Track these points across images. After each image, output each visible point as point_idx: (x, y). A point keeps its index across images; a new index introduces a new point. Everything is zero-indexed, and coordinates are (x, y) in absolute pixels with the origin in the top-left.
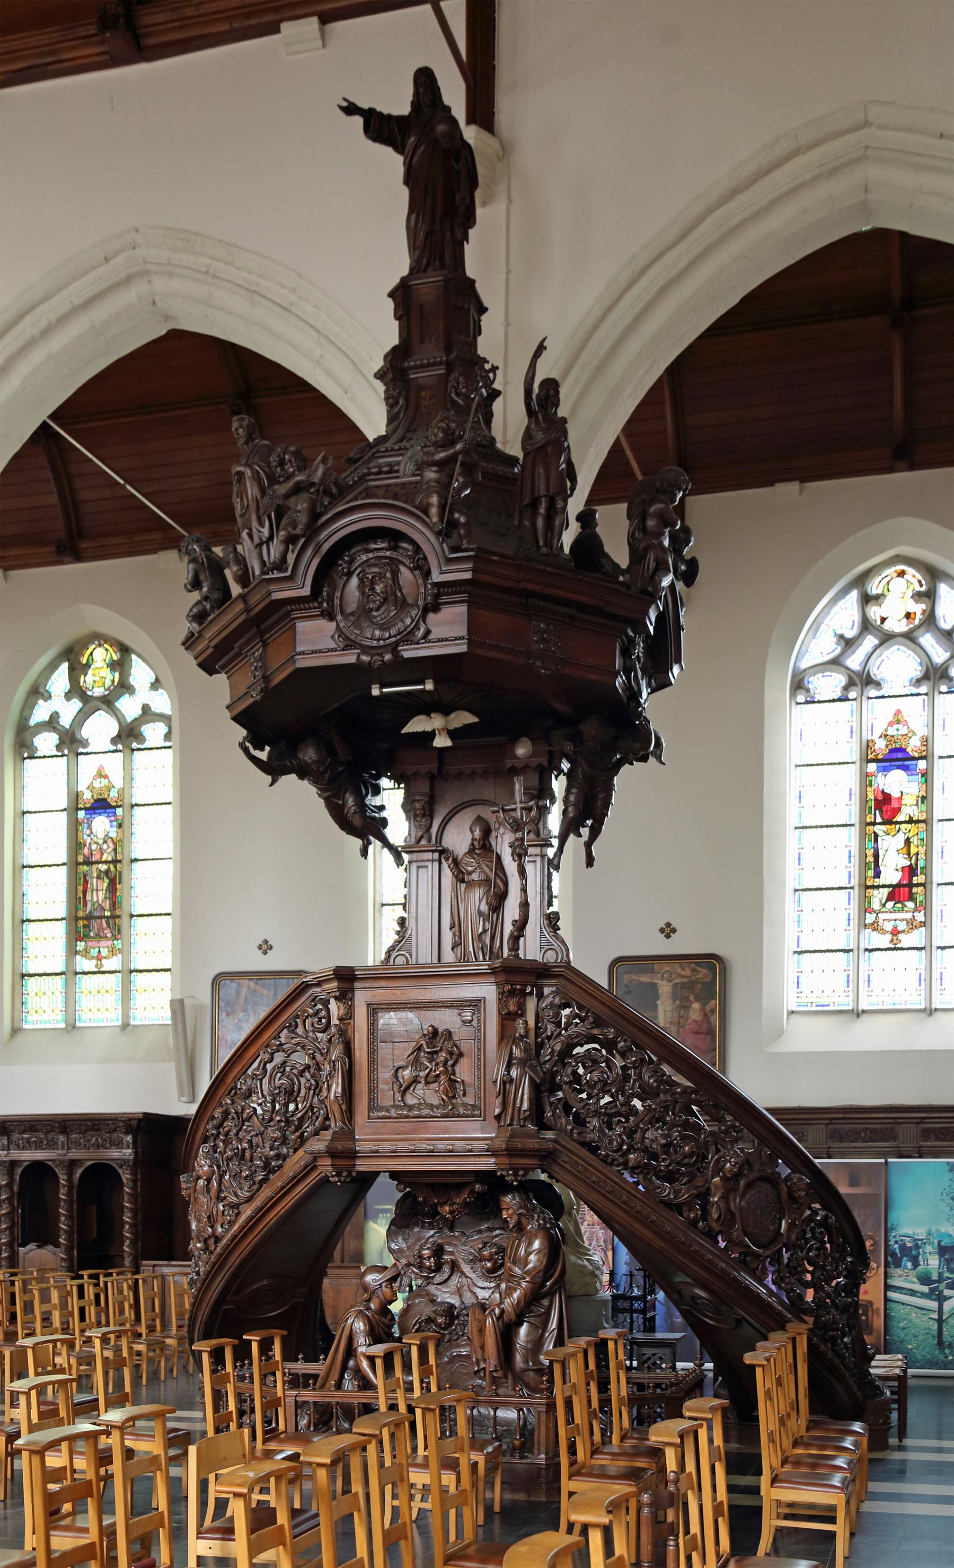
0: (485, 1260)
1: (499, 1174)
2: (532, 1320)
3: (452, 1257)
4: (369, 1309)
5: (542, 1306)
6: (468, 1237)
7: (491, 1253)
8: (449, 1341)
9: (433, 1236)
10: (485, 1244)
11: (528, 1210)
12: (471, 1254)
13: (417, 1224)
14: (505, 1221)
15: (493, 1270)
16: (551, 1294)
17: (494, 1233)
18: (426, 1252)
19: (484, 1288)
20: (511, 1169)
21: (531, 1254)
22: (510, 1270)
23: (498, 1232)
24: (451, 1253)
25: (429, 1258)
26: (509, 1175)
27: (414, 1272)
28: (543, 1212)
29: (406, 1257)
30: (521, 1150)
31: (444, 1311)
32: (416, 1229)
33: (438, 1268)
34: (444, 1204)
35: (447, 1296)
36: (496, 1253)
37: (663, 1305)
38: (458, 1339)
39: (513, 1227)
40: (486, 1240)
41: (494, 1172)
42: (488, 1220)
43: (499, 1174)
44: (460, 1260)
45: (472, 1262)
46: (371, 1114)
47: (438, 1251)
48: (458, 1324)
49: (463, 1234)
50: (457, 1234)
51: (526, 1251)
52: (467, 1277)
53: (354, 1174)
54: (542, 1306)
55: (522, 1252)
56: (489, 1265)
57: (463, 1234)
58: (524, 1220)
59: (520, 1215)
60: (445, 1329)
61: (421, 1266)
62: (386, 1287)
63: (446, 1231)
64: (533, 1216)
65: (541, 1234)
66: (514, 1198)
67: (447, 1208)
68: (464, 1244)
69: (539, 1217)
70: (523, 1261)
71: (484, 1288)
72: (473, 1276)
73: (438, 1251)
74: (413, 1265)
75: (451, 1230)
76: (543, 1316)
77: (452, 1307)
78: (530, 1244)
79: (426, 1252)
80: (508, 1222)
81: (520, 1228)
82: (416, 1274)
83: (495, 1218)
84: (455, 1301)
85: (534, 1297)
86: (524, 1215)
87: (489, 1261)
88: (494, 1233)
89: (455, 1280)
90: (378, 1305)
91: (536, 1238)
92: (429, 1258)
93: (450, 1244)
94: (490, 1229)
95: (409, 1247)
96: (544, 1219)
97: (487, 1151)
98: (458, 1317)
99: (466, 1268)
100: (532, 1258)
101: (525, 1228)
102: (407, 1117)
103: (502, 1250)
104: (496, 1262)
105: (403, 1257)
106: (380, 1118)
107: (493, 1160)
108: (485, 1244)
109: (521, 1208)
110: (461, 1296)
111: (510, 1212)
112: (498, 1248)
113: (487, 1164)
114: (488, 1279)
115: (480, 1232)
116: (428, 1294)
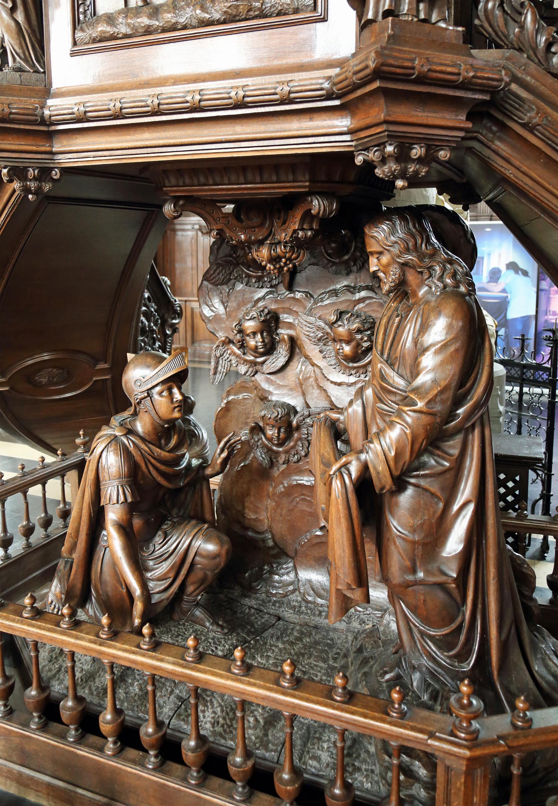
0: (341, 341)
1: (359, 160)
2: (423, 482)
3: (292, 332)
4: (130, 432)
5: (446, 455)
6: (315, 303)
7: (350, 332)
8: (287, 462)
9: (263, 298)
10: (341, 314)
11: (422, 256)
12: (319, 328)
13: (239, 279)
14: (375, 276)
15: (355, 357)
16: (465, 430)
17: (358, 296)
18: (250, 325)
19: (340, 384)
20: (392, 137)
21: (426, 350)
22: (383, 378)
23: (363, 294)
24: (290, 326)
25: (254, 333)
26: (384, 161)
27: (235, 354)
28: (451, 262)
29: (225, 329)
30: (422, 80)
31: (276, 419)
32: (240, 287)
33: (270, 349)
34: (261, 243)
35: (282, 394)
36: (359, 331)
37: (503, 340)
38: (298, 461)
39: (390, 292)
40: (342, 308)
41: (349, 156)
42: (348, 274)
43: (359, 160)
44: (304, 338)
45: (323, 340)
46: (79, 34)
47: (271, 323)
48: (300, 439)
49: (309, 295)
50: (298, 295)
51: (416, 342)
52: (313, 365)
53: (56, 174)
54: (446, 455)
55: (408, 339)
56: (347, 349)
57: (309, 295)
58: (411, 277)
59: (404, 265)
60: (280, 445)
61: (243, 346)
62: (160, 394)
63: (282, 289)
64: (430, 268)
65: (450, 306)
66: (393, 232)
67: (265, 252)
68: (310, 313)
69: (444, 270)
70: (409, 361)
71: (340, 384)
72: (322, 363)
73: (271, 323)
74: (233, 343)
75: (290, 288)
76: (448, 476)
77: (292, 410)
78: (424, 328)
79: (250, 325)
80: (379, 280)
81: (402, 290)
82: (238, 356)
83: (360, 269)
84: (296, 401)
85: (433, 437)
86: (414, 267)
87: (348, 342)
88: (358, 296)
89: (298, 367)
90: (149, 426)
91: (439, 314)
92: (254, 333)
93: (290, 311)
94: (351, 289)
95: (229, 315)
96: (454, 275)
97: (329, 97)
98: (298, 428)
99: (312, 350)
100: (428, 361)
101: (415, 294)
102: (148, 31)
103: (370, 326)
104: (358, 345)
105: (221, 329)
106: (94, 41)
107: (343, 123)
108: (341, 314)
109: (407, 250)
110: (304, 394)
111: (385, 259)
112: (363, 322)
113: (330, 133)
114: (347, 370)
115: (335, 293)
116: (257, 387)
